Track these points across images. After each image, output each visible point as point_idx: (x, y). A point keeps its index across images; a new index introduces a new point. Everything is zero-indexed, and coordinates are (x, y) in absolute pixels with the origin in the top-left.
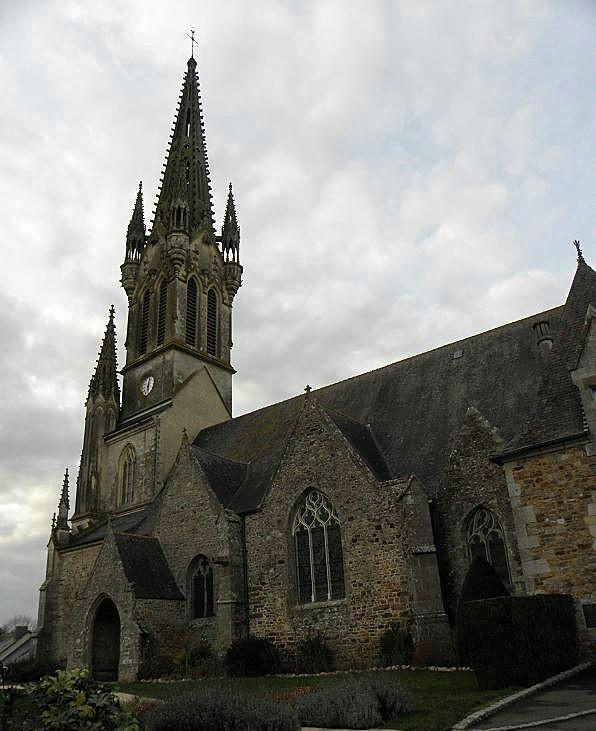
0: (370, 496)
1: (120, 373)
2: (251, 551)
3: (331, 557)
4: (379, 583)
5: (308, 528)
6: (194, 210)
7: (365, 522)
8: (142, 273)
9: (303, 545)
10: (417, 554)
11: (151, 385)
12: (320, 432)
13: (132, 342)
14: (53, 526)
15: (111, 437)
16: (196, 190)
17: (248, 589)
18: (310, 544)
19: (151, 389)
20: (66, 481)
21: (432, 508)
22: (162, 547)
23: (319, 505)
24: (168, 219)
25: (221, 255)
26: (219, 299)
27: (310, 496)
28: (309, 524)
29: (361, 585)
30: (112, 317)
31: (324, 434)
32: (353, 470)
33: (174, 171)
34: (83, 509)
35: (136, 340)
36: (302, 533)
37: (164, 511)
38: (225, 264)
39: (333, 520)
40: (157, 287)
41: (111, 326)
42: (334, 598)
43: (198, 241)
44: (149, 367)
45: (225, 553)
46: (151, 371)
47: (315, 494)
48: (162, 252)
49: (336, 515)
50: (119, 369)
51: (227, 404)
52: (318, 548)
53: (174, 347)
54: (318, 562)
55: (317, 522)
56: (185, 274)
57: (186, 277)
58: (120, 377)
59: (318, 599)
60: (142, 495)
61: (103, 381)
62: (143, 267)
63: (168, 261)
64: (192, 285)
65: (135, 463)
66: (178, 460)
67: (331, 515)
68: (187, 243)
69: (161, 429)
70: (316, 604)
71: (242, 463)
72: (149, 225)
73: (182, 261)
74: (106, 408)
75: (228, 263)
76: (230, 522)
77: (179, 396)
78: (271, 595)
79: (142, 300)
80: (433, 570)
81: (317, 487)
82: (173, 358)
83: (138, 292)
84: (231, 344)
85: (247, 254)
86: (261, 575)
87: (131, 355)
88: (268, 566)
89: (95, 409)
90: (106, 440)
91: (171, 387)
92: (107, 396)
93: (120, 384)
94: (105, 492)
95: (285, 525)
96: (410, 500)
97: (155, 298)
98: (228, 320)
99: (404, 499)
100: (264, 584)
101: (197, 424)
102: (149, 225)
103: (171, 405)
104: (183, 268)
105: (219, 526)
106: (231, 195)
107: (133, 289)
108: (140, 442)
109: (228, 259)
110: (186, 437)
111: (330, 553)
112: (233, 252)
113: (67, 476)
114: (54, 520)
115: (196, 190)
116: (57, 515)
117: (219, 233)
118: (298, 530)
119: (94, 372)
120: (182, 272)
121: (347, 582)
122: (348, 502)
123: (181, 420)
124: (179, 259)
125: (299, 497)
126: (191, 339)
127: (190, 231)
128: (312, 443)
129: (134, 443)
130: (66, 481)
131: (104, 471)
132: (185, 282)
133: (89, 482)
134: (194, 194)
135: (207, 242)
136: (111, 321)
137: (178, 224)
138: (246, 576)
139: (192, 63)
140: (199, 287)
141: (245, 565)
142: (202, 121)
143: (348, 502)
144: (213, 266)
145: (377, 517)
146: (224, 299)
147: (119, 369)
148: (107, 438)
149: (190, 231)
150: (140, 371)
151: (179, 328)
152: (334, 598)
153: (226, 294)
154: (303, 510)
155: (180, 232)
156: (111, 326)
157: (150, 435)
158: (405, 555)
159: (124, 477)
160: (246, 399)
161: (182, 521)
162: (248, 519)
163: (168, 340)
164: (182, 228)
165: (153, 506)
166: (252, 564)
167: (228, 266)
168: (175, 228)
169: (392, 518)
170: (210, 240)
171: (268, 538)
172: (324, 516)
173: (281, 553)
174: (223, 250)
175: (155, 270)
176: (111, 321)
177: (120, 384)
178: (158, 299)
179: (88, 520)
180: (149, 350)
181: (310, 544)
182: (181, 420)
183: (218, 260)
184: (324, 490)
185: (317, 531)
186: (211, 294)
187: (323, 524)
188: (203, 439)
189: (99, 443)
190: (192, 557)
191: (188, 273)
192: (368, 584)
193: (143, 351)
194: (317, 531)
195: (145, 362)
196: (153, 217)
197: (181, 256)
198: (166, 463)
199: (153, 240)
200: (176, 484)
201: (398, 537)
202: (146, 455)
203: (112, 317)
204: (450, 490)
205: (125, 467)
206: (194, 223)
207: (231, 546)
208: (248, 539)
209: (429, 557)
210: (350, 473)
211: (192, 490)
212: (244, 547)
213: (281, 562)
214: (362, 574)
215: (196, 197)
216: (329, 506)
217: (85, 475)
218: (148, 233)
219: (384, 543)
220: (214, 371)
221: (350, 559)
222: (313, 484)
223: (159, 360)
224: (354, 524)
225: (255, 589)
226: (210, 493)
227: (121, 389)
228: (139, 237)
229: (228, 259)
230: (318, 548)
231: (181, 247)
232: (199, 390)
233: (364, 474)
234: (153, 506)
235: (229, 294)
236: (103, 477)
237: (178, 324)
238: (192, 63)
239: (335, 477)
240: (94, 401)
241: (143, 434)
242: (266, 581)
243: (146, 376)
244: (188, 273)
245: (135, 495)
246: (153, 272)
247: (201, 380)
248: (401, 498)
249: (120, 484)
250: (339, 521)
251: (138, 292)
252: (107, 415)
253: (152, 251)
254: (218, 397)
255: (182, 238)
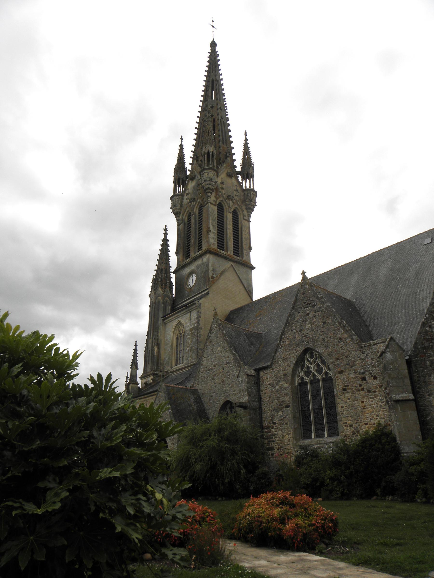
0: (355, 354)
1: (173, 273)
2: (265, 398)
3: (326, 403)
4: (366, 424)
5: (307, 380)
6: (220, 153)
7: (352, 375)
8: (185, 201)
9: (304, 395)
10: (397, 401)
11: (194, 280)
12: (314, 305)
13: (181, 250)
14: (127, 381)
15: (167, 318)
16: (221, 137)
17: (262, 427)
18: (310, 393)
19: (194, 282)
20: (136, 350)
21: (409, 363)
22: (201, 395)
23: (315, 362)
24: (201, 161)
25: (240, 185)
26: (240, 216)
27: (308, 356)
28: (308, 377)
29: (351, 426)
30: (166, 234)
31: (317, 307)
32: (341, 333)
33: (204, 126)
34: (148, 370)
35: (184, 248)
36: (303, 384)
37: (202, 369)
38: (244, 191)
39: (326, 373)
40: (196, 211)
41: (165, 241)
42: (329, 435)
43: (223, 175)
44: (193, 267)
45: (245, 399)
46: (194, 269)
47: (312, 354)
48: (198, 185)
49: (329, 369)
50: (172, 270)
51: (250, 293)
52: (316, 396)
53: (209, 252)
54: (316, 407)
55: (314, 375)
56: (215, 199)
57: (216, 202)
58: (173, 276)
59: (317, 436)
60: (188, 359)
61: (161, 279)
62: (186, 197)
63: (204, 190)
64: (221, 208)
65: (184, 335)
66: (210, 331)
67: (325, 369)
68: (215, 177)
69: (202, 310)
70: (316, 440)
71: (249, 328)
72: (188, 167)
73: (212, 190)
74: (164, 296)
75: (246, 189)
76: (248, 375)
77: (214, 287)
78: (280, 433)
79: (186, 220)
80: (412, 415)
81: (313, 348)
82: (208, 260)
83: (183, 215)
84: (250, 248)
85: (259, 182)
86: (272, 417)
87: (181, 259)
88: (277, 410)
89: (156, 298)
90: (163, 320)
91: (207, 280)
92: (163, 289)
93: (173, 280)
94: (164, 356)
95: (290, 377)
96: (389, 356)
97: (195, 218)
98: (248, 231)
99: (384, 355)
100: (274, 423)
101: (226, 306)
102: (188, 167)
103: (208, 293)
104: (214, 194)
105: (240, 379)
106: (246, 140)
107: (180, 213)
108: (187, 320)
109: (246, 187)
110: (216, 314)
111: (326, 399)
112: (250, 182)
113: (136, 346)
114: (127, 377)
115: (221, 137)
116: (129, 374)
117: (238, 169)
118: (300, 382)
119: (154, 273)
120: (213, 198)
121: (340, 424)
122: (338, 359)
123: (219, 302)
124: (210, 189)
125: (300, 356)
126: (221, 244)
127: (217, 168)
128: (308, 314)
129: (183, 321)
130: (136, 350)
131: (163, 342)
132: (215, 205)
133: (153, 350)
134: (219, 141)
135: (230, 176)
136: (165, 237)
137: (208, 165)
138: (261, 418)
139: (213, 45)
140: (226, 208)
141: (260, 408)
142: (223, 92)
143: (338, 359)
144: (235, 193)
145: (362, 371)
146: (244, 216)
147: (172, 270)
148: (165, 318)
149: (217, 168)
150: (186, 271)
151: (212, 240)
152: (329, 435)
153: (245, 212)
154: (303, 366)
155: (209, 169)
156: (165, 241)
157: (194, 315)
158: (387, 402)
159: (177, 346)
160: (263, 285)
161: (214, 376)
162: (261, 373)
163: (204, 247)
164: (211, 166)
165: (196, 366)
166: (266, 408)
167: (246, 192)
168: (206, 167)
169: (375, 371)
170: (233, 174)
171: (277, 387)
172: (319, 370)
173: (287, 399)
174: (242, 180)
175: (194, 199)
176: (165, 237)
177: (173, 280)
178: (197, 219)
179: (152, 377)
180: (193, 255)
181: (310, 393)
182: (219, 302)
183: (238, 188)
184: (319, 350)
185: (314, 382)
186: (235, 214)
187: (319, 377)
188: (231, 317)
189: (159, 322)
190: (222, 402)
191: (217, 199)
192: (357, 425)
193: (188, 256)
194: (314, 382)
195: (189, 264)
196: (191, 161)
197: (211, 187)
198: (204, 332)
199: (192, 177)
200: (210, 348)
201: (381, 386)
202: (191, 330)
203: (166, 234)
204: (424, 348)
205: (177, 338)
206: (220, 163)
207: (249, 395)
208: (262, 389)
209: (249, 299)
210: (339, 336)
211: (219, 354)
212: (259, 395)
213: (288, 406)
214: (352, 416)
215: (221, 143)
216: (323, 362)
217: (150, 346)
218: (188, 173)
219: (369, 391)
220: (241, 270)
221: (341, 405)
222: (311, 346)
223: (199, 262)
224: (343, 376)
225: (268, 427)
226: (233, 354)
227: (174, 284)
228: (181, 176)
229: (246, 187)
230: (316, 396)
231: (211, 180)
232: (228, 281)
233: (350, 336)
234: (196, 366)
235: (248, 212)
236: (162, 346)
237: (211, 235)
238: (213, 45)
239: (327, 340)
240: (155, 294)
241: (189, 313)
242: (277, 421)
243: (191, 274)
244: (217, 199)
245: (184, 359)
246: (193, 200)
247: (230, 276)
248: (381, 355)
249: (174, 352)
250: (331, 374)
251: (183, 215)
252: (165, 303)
253: (191, 185)
254: (241, 287)
255: (212, 174)
